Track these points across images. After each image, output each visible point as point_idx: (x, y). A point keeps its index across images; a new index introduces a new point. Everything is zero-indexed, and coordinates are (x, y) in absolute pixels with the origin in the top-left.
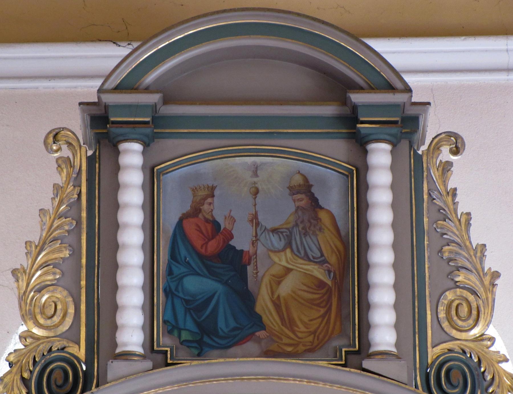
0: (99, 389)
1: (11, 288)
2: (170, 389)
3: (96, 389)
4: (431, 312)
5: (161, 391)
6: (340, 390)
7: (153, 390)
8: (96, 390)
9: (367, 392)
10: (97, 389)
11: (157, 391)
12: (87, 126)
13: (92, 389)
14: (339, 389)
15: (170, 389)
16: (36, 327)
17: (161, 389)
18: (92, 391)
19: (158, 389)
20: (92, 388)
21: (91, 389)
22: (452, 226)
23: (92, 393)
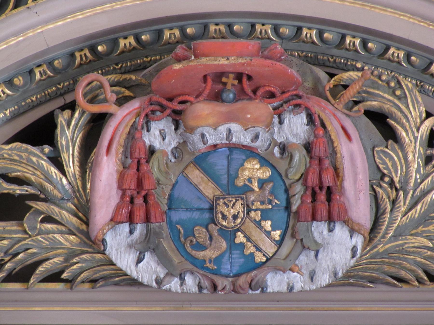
0: (37, 3)
1: (20, 89)
2: (131, 4)
3: (33, 2)
4: (284, 293)
5: (118, 6)
6: (353, 6)
7: (108, 5)
8: (33, 4)
9: (352, 1)
10: (34, 3)
11: (113, 6)
12: (215, 187)
13: (28, 3)
14: (352, 5)
15: (131, 4)
16: (5, 182)
17: (119, 3)
18: (27, 6)
19: (114, 4)
20: (28, 2)
21: (27, 4)
22: (11, 160)
23: (28, 8)
